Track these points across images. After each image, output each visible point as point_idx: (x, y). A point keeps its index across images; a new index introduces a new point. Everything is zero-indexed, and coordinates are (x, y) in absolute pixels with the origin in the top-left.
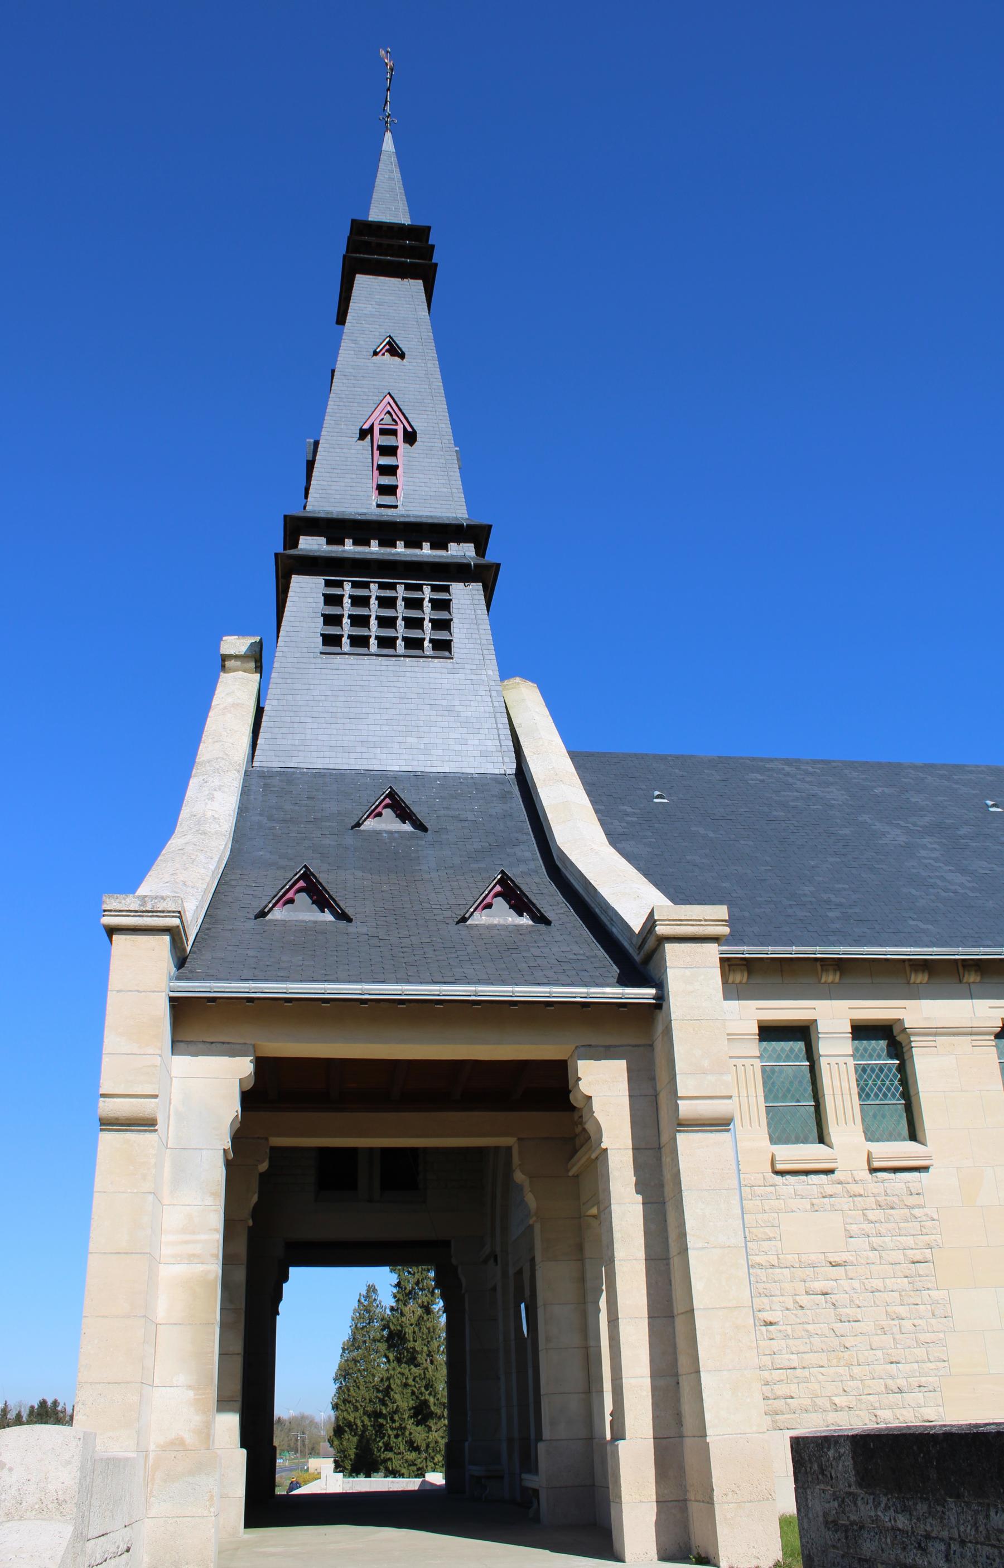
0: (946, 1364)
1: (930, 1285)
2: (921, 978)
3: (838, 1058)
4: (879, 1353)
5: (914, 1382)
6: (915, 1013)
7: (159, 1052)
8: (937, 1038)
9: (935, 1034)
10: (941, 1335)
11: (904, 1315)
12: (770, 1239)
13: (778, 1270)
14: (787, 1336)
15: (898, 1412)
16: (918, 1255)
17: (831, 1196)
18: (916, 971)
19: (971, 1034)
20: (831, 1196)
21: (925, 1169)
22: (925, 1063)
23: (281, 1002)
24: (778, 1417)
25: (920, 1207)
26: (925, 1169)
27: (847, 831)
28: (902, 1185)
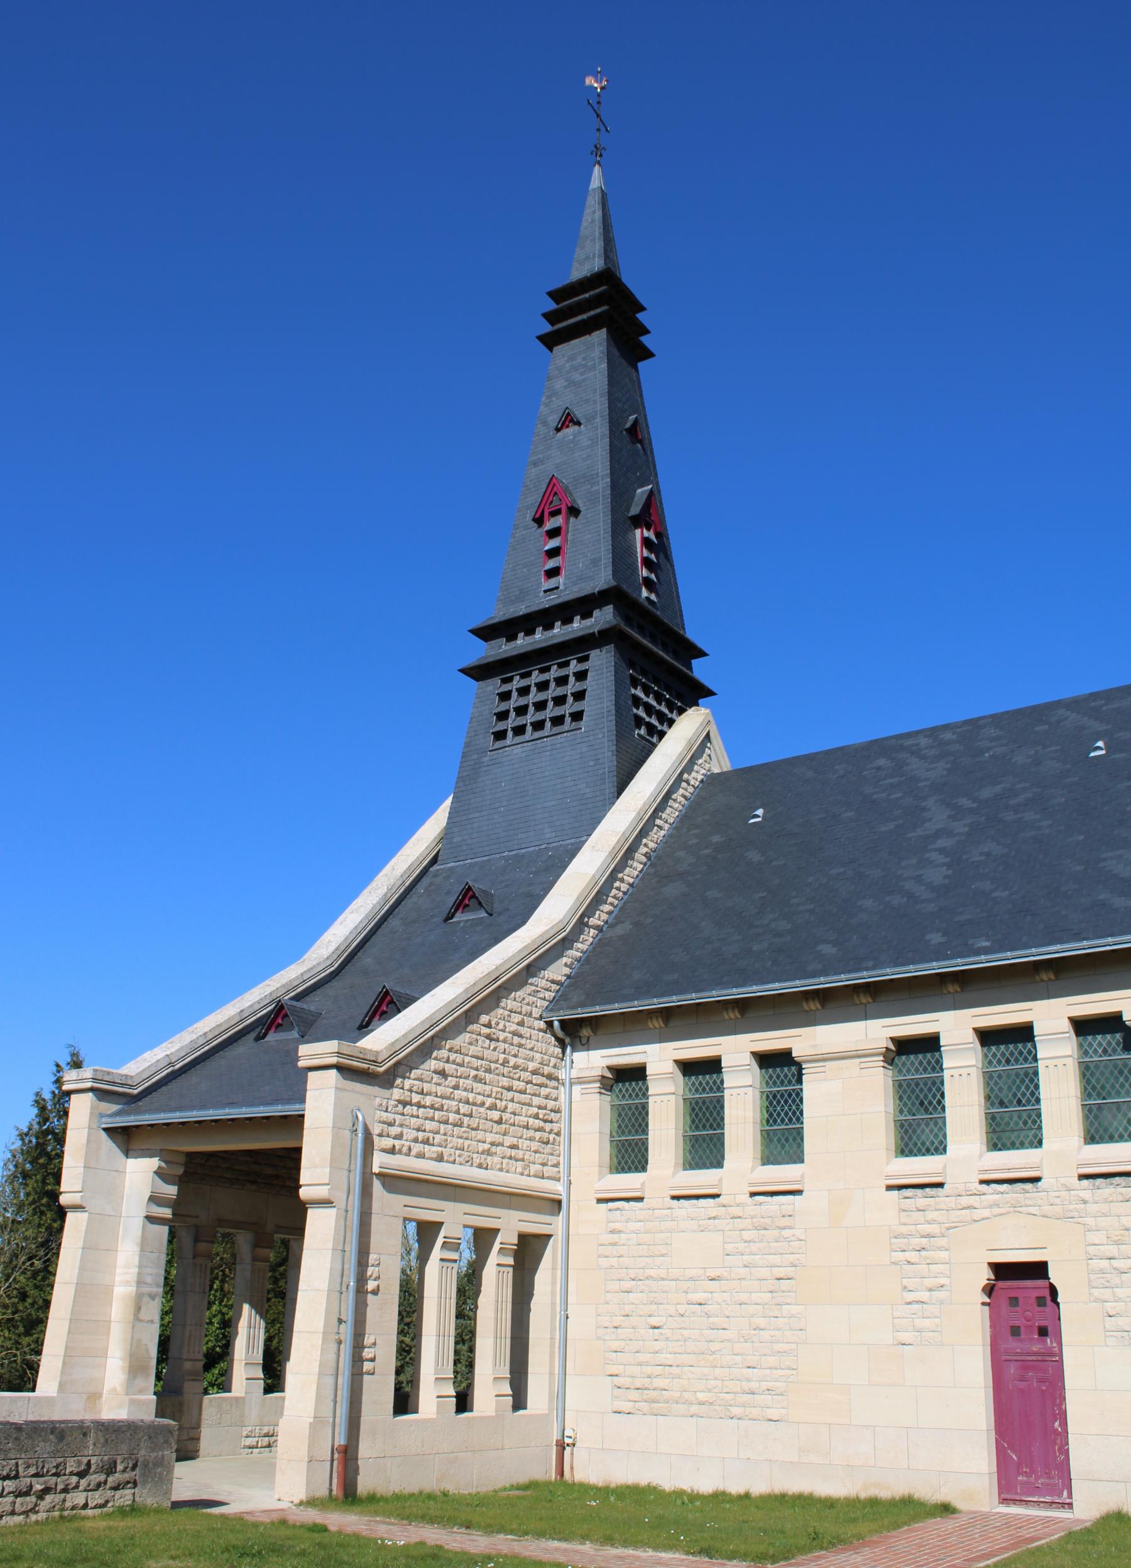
0: (794, 1372)
1: (789, 1301)
2: (814, 1005)
3: (742, 1098)
4: (738, 1358)
5: (764, 1385)
6: (800, 1040)
7: (896, 1321)
8: (828, 1063)
9: (824, 1060)
10: (794, 1346)
11: (762, 1326)
12: (663, 1255)
13: (781, 1319)
14: (667, 1339)
15: (748, 1410)
16: (780, 1272)
17: (714, 1218)
18: (807, 1000)
19: (859, 1057)
20: (714, 1218)
21: (799, 1192)
22: (816, 1091)
23: (247, 1046)
24: (654, 1405)
25: (791, 1228)
26: (799, 1192)
27: (706, 852)
28: (777, 1207)
